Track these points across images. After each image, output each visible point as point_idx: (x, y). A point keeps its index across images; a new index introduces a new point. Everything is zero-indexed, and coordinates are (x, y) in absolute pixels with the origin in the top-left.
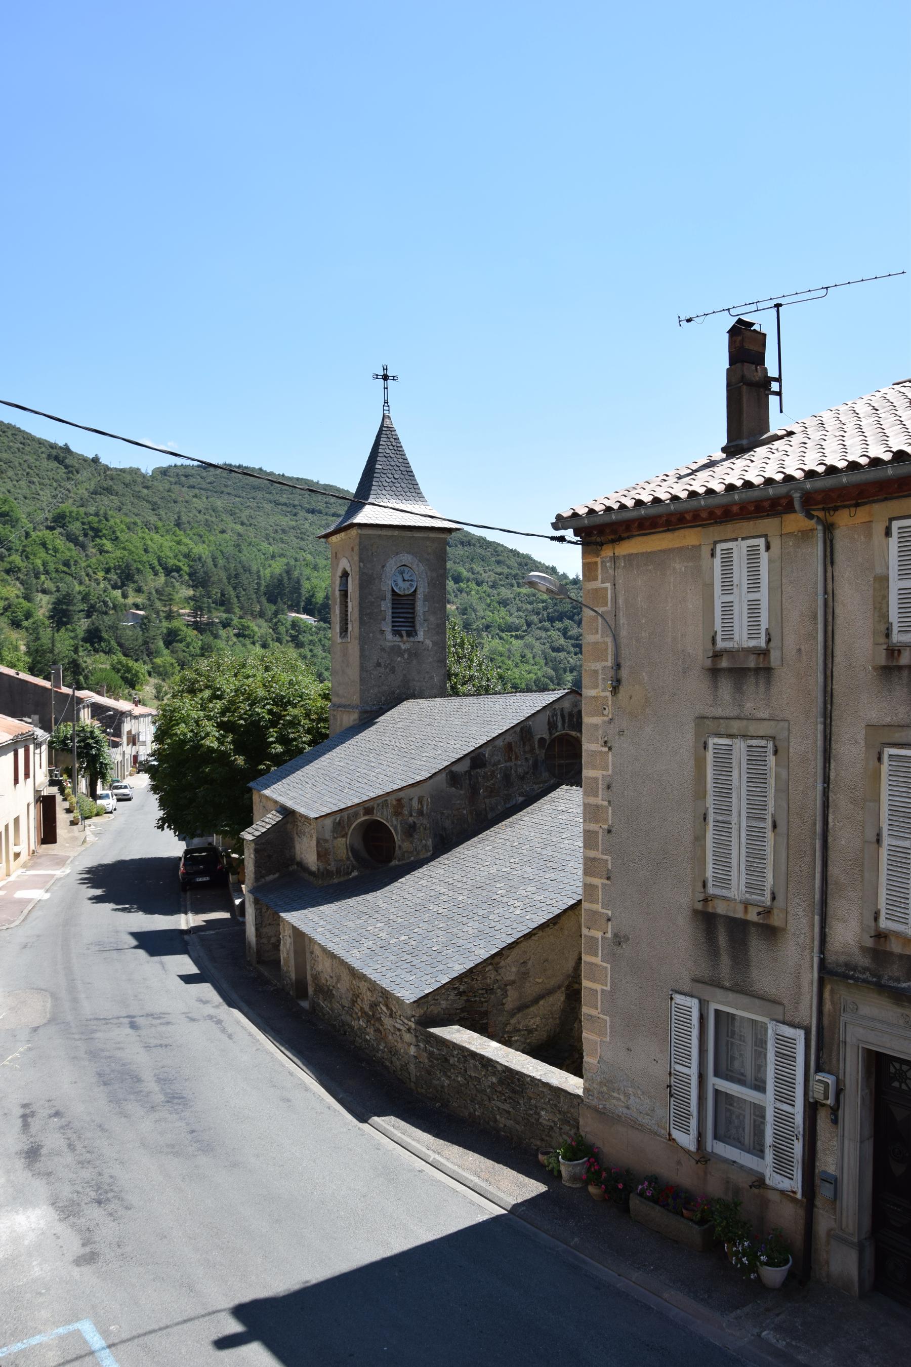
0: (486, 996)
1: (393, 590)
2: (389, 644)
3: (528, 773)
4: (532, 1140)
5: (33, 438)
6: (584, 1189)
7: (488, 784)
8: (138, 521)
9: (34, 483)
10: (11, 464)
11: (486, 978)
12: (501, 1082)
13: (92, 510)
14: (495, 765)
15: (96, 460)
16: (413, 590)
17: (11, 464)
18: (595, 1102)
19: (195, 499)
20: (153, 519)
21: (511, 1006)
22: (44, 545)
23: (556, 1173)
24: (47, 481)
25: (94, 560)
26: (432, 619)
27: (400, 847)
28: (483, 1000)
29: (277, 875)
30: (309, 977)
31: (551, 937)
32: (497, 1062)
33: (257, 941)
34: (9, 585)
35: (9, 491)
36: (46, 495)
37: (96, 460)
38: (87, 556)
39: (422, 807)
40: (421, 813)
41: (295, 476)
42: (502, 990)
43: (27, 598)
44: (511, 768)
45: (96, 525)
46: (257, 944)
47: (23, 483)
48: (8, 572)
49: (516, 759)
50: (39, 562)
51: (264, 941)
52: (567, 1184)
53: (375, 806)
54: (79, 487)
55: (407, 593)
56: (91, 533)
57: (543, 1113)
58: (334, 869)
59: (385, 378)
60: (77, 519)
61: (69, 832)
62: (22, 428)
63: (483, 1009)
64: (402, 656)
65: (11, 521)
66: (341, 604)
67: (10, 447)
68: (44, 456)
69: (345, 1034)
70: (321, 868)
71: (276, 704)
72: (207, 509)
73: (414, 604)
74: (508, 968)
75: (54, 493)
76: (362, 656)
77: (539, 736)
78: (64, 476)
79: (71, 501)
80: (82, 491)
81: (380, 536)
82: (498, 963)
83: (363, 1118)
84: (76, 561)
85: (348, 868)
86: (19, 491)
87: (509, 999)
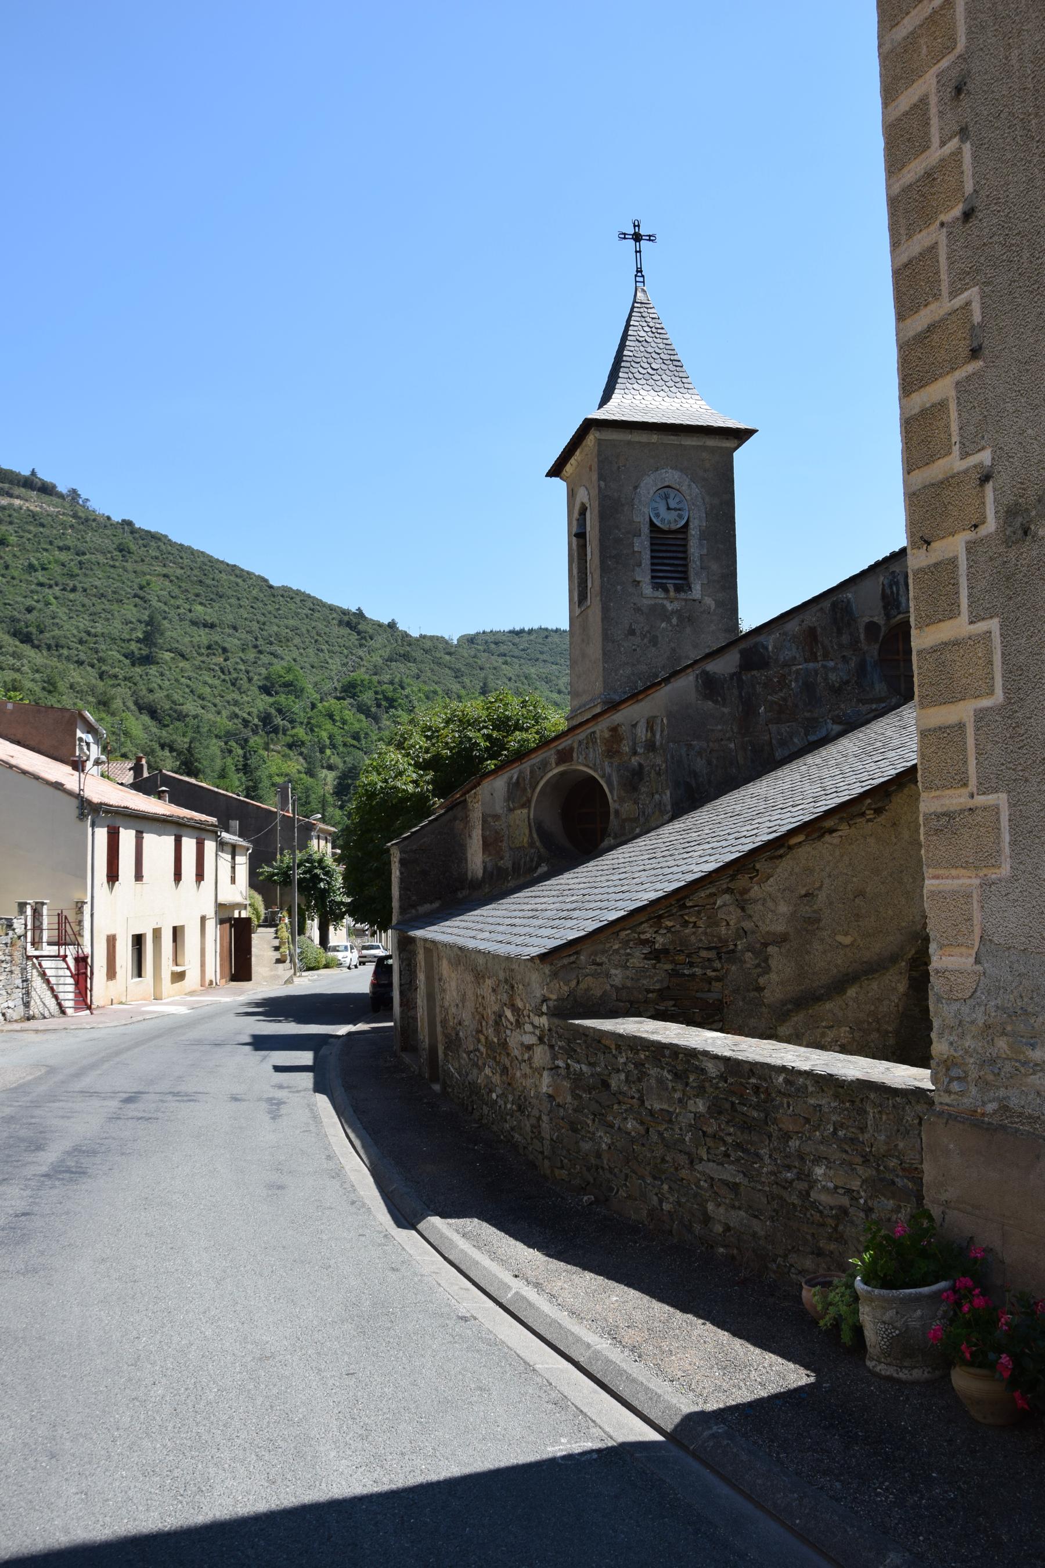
0: (717, 964)
2: (645, 601)
3: (847, 682)
4: (793, 1258)
5: (324, 605)
6: (941, 1384)
7: (774, 698)
9: (322, 651)
11: (717, 924)
12: (716, 1110)
13: (386, 678)
14: (786, 665)
15: (392, 625)
16: (683, 522)
18: (971, 1098)
20: (455, 687)
22: (331, 716)
23: (846, 1337)
24: (337, 648)
26: (714, 567)
27: (617, 812)
28: (711, 973)
32: (705, 1053)
35: (295, 660)
36: (335, 664)
37: (392, 625)
38: (379, 728)
39: (654, 734)
40: (651, 746)
45: (390, 695)
48: (290, 746)
50: (324, 735)
52: (881, 1368)
53: (576, 745)
54: (372, 654)
55: (674, 527)
56: (384, 703)
57: (819, 1171)
59: (637, 237)
60: (370, 688)
61: (271, 970)
62: (312, 595)
63: (711, 997)
64: (669, 621)
65: (295, 691)
67: (297, 614)
70: (489, 865)
71: (496, 728)
72: (518, 676)
73: (685, 546)
74: (770, 904)
75: (345, 660)
76: (606, 618)
77: (867, 619)
79: (363, 669)
80: (377, 659)
81: (629, 443)
82: (745, 891)
85: (532, 860)
86: (306, 659)
87: (774, 977)
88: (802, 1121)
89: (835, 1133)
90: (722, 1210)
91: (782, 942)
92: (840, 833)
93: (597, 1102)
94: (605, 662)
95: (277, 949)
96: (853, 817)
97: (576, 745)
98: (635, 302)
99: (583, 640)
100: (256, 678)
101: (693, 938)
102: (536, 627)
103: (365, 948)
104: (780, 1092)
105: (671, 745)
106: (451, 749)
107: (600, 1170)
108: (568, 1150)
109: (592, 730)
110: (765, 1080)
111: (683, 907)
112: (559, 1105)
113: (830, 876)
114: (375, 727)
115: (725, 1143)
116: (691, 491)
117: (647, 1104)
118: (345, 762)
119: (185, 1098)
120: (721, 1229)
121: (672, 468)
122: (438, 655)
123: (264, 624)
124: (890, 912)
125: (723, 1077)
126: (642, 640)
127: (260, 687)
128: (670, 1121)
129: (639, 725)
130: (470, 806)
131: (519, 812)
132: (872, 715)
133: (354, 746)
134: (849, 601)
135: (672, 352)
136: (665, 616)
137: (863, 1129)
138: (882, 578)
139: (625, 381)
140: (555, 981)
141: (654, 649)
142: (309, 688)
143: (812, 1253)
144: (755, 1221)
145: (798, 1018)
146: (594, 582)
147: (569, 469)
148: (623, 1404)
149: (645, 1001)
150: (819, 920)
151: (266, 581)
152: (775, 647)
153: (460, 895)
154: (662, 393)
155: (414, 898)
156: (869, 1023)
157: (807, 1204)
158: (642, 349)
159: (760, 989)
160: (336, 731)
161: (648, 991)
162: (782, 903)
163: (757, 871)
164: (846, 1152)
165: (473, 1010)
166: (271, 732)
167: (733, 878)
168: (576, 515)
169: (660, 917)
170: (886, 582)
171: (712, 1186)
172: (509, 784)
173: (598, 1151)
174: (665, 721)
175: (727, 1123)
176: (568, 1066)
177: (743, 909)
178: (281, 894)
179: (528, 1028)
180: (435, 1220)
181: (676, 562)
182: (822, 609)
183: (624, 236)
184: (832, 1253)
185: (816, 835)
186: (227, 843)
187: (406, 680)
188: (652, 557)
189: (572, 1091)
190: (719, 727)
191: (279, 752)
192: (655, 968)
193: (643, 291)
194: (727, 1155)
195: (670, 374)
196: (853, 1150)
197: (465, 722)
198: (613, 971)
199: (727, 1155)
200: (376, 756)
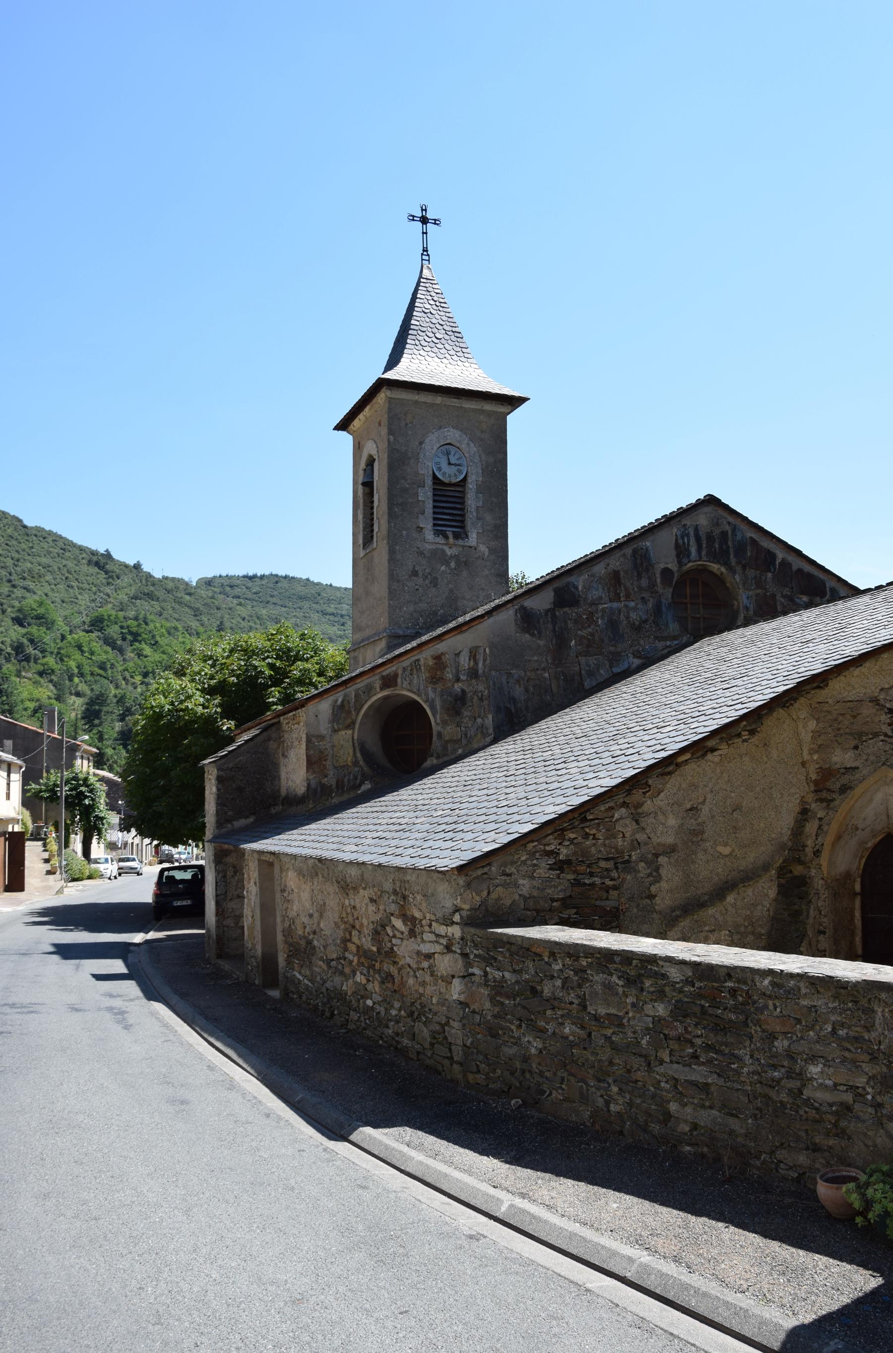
0: (614, 874)
1: (435, 477)
2: (428, 546)
3: (646, 621)
4: (781, 1154)
5: (75, 545)
7: (583, 633)
8: (179, 626)
9: (72, 587)
10: (50, 569)
11: (614, 836)
12: (680, 1011)
13: (131, 614)
14: (593, 604)
15: (137, 567)
16: (462, 477)
17: (50, 569)
19: (238, 607)
20: (194, 624)
21: (668, 902)
22: (79, 647)
24: (86, 586)
25: (131, 664)
26: (488, 517)
27: (440, 735)
28: (609, 883)
29: (251, 820)
31: (746, 759)
33: (217, 921)
34: (41, 687)
35: (46, 595)
36: (84, 600)
37: (137, 567)
38: (124, 660)
39: (476, 663)
40: (473, 674)
41: (343, 586)
42: (649, 863)
43: (58, 698)
44: (619, 611)
45: (134, 629)
46: (217, 927)
47: (61, 587)
48: (41, 674)
49: (628, 596)
50: (73, 664)
51: (230, 922)
53: (400, 672)
54: (119, 592)
55: (454, 480)
56: (129, 637)
57: (814, 1070)
58: (333, 782)
59: (424, 220)
60: (116, 623)
61: (43, 881)
62: (64, 535)
63: (609, 905)
67: (49, 553)
68: (84, 561)
69: (332, 1015)
70: (313, 782)
72: (251, 616)
73: (463, 498)
74: (661, 817)
75: (93, 597)
76: (392, 560)
77: (662, 566)
78: (104, 581)
79: (110, 606)
80: (123, 597)
81: (416, 402)
82: (639, 805)
83: (337, 1131)
84: (112, 664)
85: (356, 778)
86: (56, 595)
87: (664, 885)
88: (793, 1021)
89: (834, 1032)
90: (689, 1110)
91: (670, 852)
92: (720, 752)
93: (524, 1007)
94: (390, 599)
95: (47, 861)
96: (731, 737)
97: (400, 672)
98: (421, 277)
99: (367, 579)
100: (9, 610)
101: (593, 849)
102: (267, 573)
103: (121, 860)
104: (764, 994)
105: (493, 673)
106: (238, 677)
107: (528, 1075)
108: (486, 1056)
109: (416, 658)
110: (745, 983)
111: (585, 820)
112: (474, 1012)
113: (712, 791)
114: (120, 658)
115: (692, 1045)
116: (470, 449)
117: (590, 1009)
118: (92, 690)
119: (25, 1010)
120: (687, 1129)
121: (453, 427)
122: (179, 595)
123: (18, 560)
124: (762, 825)
125: (688, 982)
126: (424, 580)
127: (13, 619)
128: (621, 1025)
129: (462, 654)
130: (285, 727)
131: (343, 733)
132: (666, 651)
133: (101, 676)
134: (647, 549)
135: (454, 325)
136: (445, 560)
137: (868, 1028)
138: (675, 530)
139: (412, 347)
140: (468, 891)
141: (434, 590)
142: (60, 622)
143: (807, 1149)
144: (731, 1121)
145: (685, 923)
146: (381, 526)
147: (356, 423)
148: (701, 1321)
149: (550, 910)
150: (703, 832)
151: (20, 521)
152: (584, 587)
153: (273, 811)
154: (444, 360)
155: (230, 813)
156: (746, 927)
157: (799, 1102)
158: (428, 320)
159: (652, 897)
160: (85, 662)
161: (553, 900)
162: (671, 816)
163: (650, 786)
164: (849, 1050)
165: (337, 920)
166: (23, 660)
167: (629, 793)
168: (363, 465)
169: (563, 830)
170: (679, 533)
171: (675, 1086)
172: (333, 708)
173: (525, 1055)
174: (487, 651)
175: (696, 1025)
176: (486, 974)
177: (637, 822)
178: (46, 811)
179: (428, 937)
180: (368, 1130)
181: (455, 512)
182: (624, 554)
183: (412, 218)
184: (831, 1147)
185: (700, 754)
186: (4, 761)
187: (150, 617)
188: (434, 507)
189: (492, 999)
190: (536, 658)
191: (30, 679)
192: (558, 877)
193: (428, 268)
194: (695, 1056)
195: (452, 343)
196: (857, 1048)
197: (249, 652)
198: (521, 882)
199: (695, 1056)
200: (162, 681)
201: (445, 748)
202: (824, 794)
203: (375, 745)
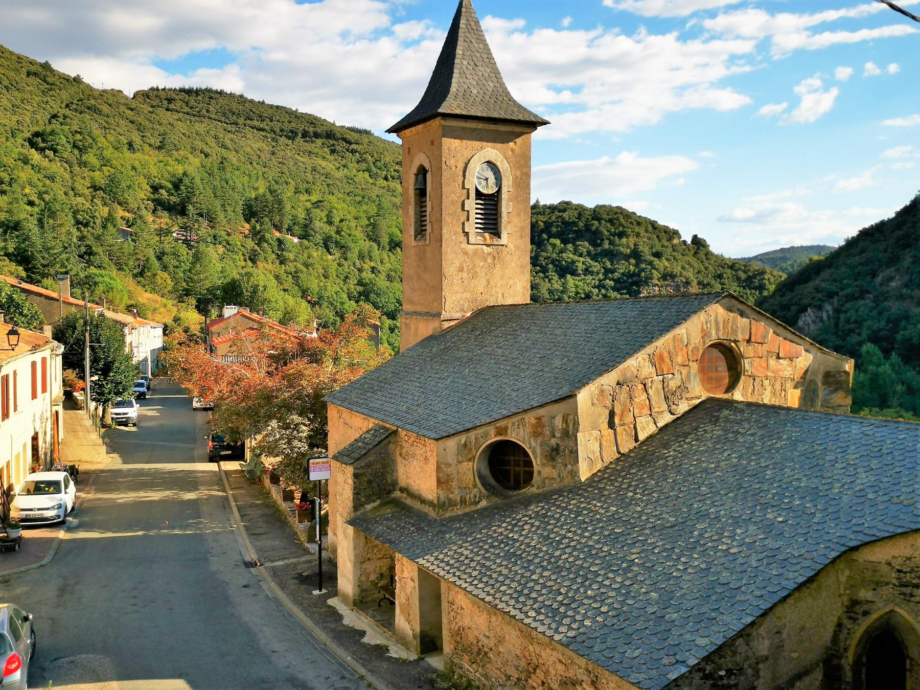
1: (477, 190)
27: (539, 472)
29: (378, 502)
30: (445, 632)
39: (568, 426)
53: (510, 425)
64: (485, 260)
66: (416, 204)
81: (463, 128)
85: (475, 497)
87: (761, 680)
177: (748, 645)
201: (544, 482)
202: (853, 615)
203: (486, 472)
